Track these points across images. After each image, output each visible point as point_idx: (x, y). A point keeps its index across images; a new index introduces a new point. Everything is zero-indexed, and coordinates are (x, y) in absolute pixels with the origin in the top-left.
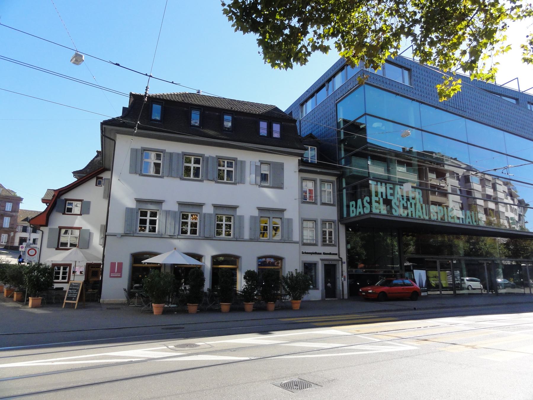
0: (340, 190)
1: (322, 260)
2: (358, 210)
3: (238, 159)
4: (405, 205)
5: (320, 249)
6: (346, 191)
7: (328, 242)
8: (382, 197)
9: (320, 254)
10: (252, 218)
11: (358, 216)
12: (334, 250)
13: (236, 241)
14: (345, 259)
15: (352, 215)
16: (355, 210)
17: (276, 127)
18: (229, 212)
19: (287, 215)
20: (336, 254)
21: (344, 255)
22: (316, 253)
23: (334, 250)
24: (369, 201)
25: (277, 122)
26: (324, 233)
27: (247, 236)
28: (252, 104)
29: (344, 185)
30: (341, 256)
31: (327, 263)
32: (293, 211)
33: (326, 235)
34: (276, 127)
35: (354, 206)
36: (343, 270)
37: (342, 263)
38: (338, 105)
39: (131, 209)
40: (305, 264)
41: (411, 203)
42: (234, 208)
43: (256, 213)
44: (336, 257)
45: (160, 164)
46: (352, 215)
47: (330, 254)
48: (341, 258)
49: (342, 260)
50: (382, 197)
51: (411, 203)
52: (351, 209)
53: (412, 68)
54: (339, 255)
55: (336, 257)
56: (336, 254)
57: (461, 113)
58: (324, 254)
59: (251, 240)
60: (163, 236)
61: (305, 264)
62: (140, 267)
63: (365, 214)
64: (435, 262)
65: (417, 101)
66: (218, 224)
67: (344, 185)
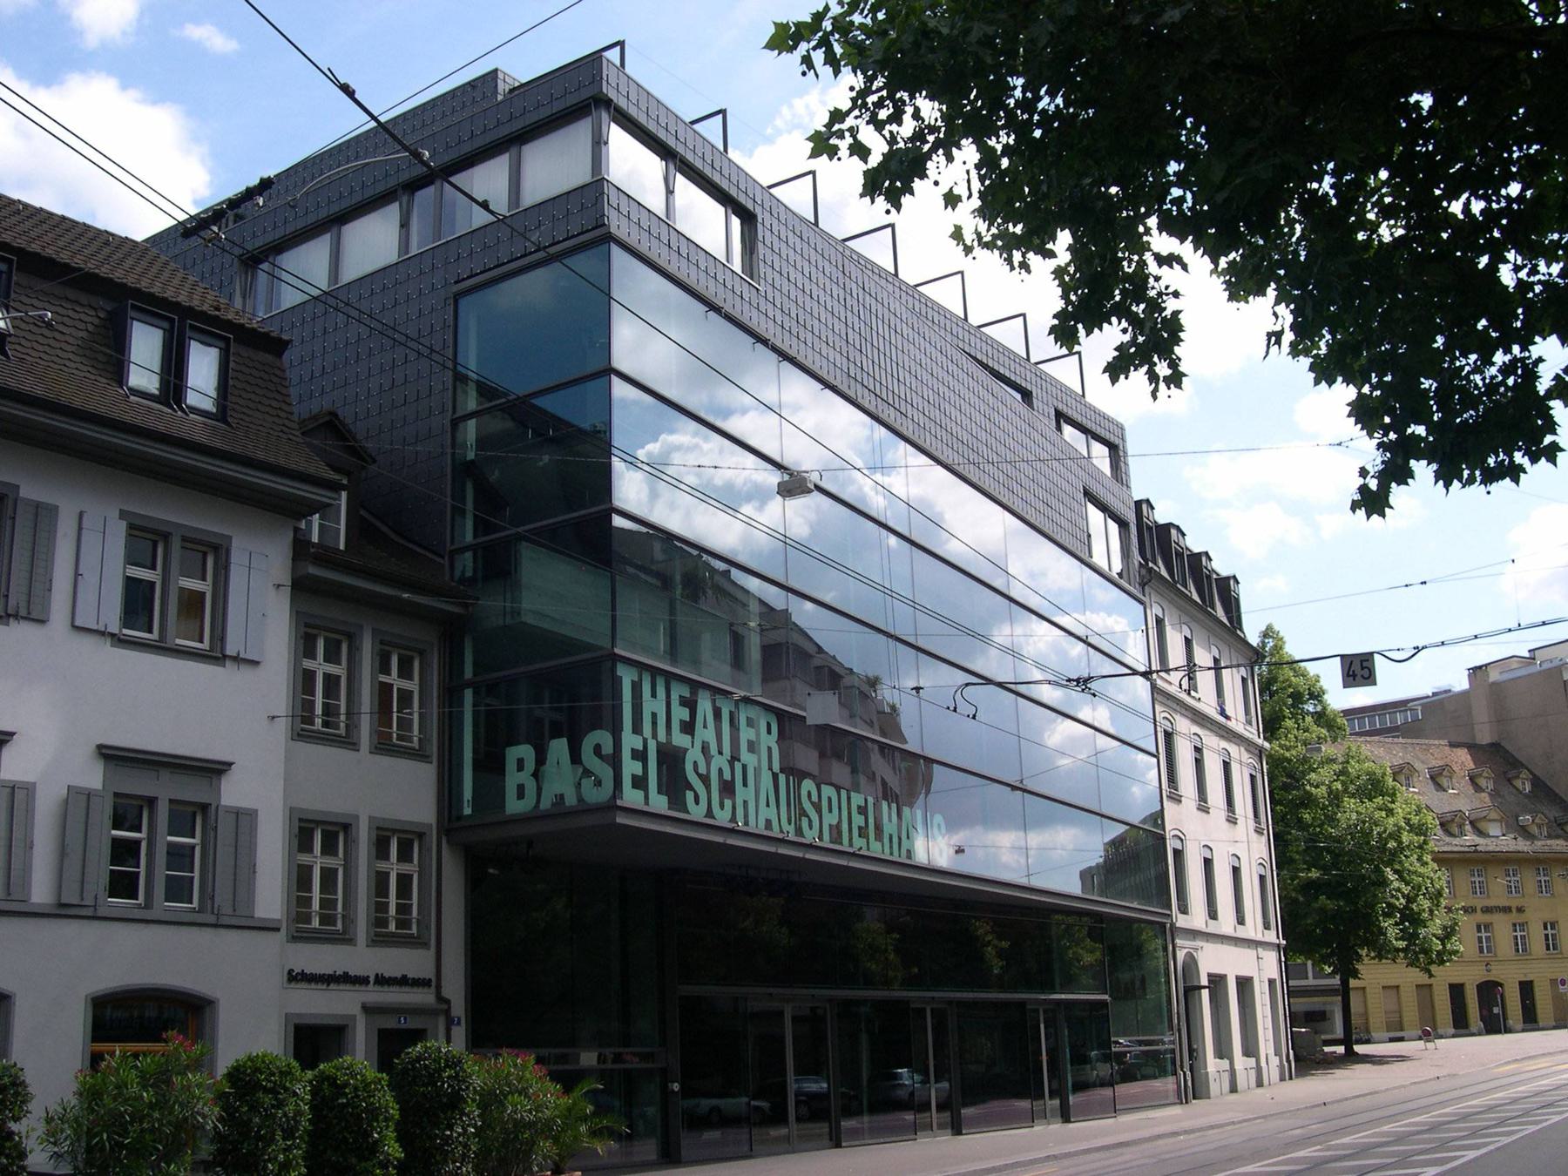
0: (451, 694)
1: (367, 1009)
2: (544, 780)
3: (23, 493)
4: (727, 776)
5: (361, 958)
6: (476, 693)
7: (392, 927)
8: (655, 736)
9: (364, 981)
10: (78, 798)
11: (546, 816)
12: (414, 962)
13: (215, 926)
14: (459, 1008)
15: (514, 806)
16: (531, 786)
17: (203, 368)
18: (191, 790)
19: (232, 793)
20: (424, 983)
21: (455, 989)
22: (346, 979)
23: (414, 962)
24: (608, 749)
25: (208, 339)
26: (381, 881)
27: (41, 892)
28: (63, 224)
29: (468, 673)
30: (446, 993)
31: (390, 1023)
32: (265, 778)
33: (310, 890)
34: (203, 368)
35: (530, 765)
36: (544, 1052)
37: (450, 1022)
38: (463, 303)
39: (89, 795)
40: (299, 1029)
41: (744, 767)
42: (215, 770)
43: (93, 777)
44: (424, 997)
45: (152, 584)
46: (514, 806)
47: (403, 981)
48: (448, 1002)
49: (447, 1012)
50: (655, 736)
51: (744, 767)
52: (513, 779)
53: (758, 211)
54: (439, 987)
55: (424, 997)
56: (424, 983)
57: (889, 415)
58: (381, 981)
59: (62, 911)
60: (225, 920)
61: (299, 1029)
62: (783, 1072)
63: (584, 809)
64: (781, 1014)
65: (774, 349)
66: (116, 842)
67: (468, 673)
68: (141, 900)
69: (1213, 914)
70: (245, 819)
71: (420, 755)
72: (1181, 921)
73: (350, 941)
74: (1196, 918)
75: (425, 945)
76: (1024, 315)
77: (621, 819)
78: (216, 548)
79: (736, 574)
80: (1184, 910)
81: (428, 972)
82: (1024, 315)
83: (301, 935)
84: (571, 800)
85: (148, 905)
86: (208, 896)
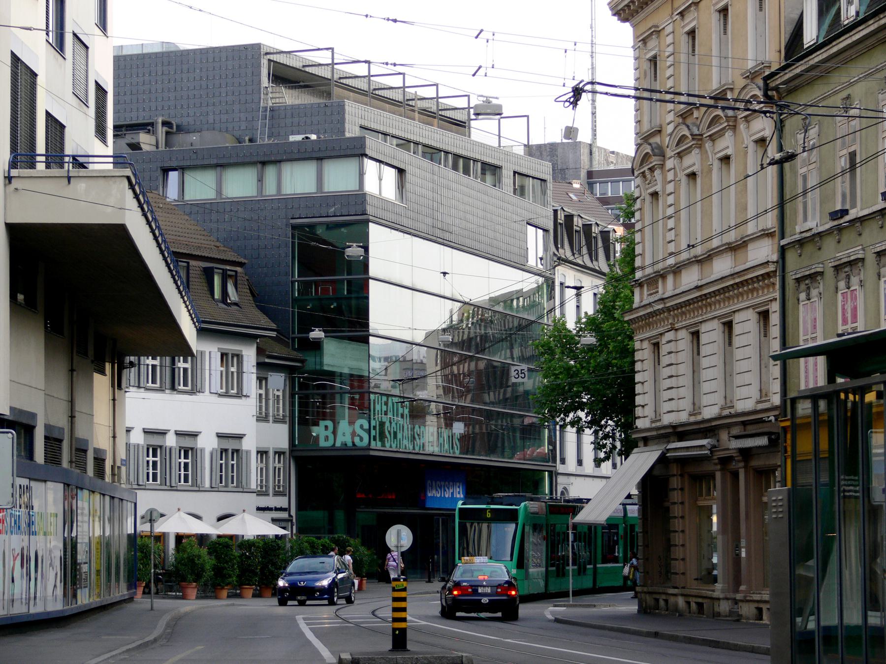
11: (338, 449)
12: (282, 502)
13: (199, 491)
16: (331, 437)
23: (282, 502)
35: (331, 428)
49: (292, 521)
58: (277, 509)
59: (212, 489)
68: (190, 483)
69: (580, 462)
70: (248, 452)
71: (282, 421)
72: (560, 468)
73: (268, 495)
74: (571, 466)
75: (285, 495)
76: (528, 116)
77: (372, 453)
78: (238, 355)
79: (307, 69)
80: (563, 461)
81: (286, 506)
82: (528, 116)
83: (260, 494)
84: (350, 444)
85: (226, 486)
86: (195, 479)
